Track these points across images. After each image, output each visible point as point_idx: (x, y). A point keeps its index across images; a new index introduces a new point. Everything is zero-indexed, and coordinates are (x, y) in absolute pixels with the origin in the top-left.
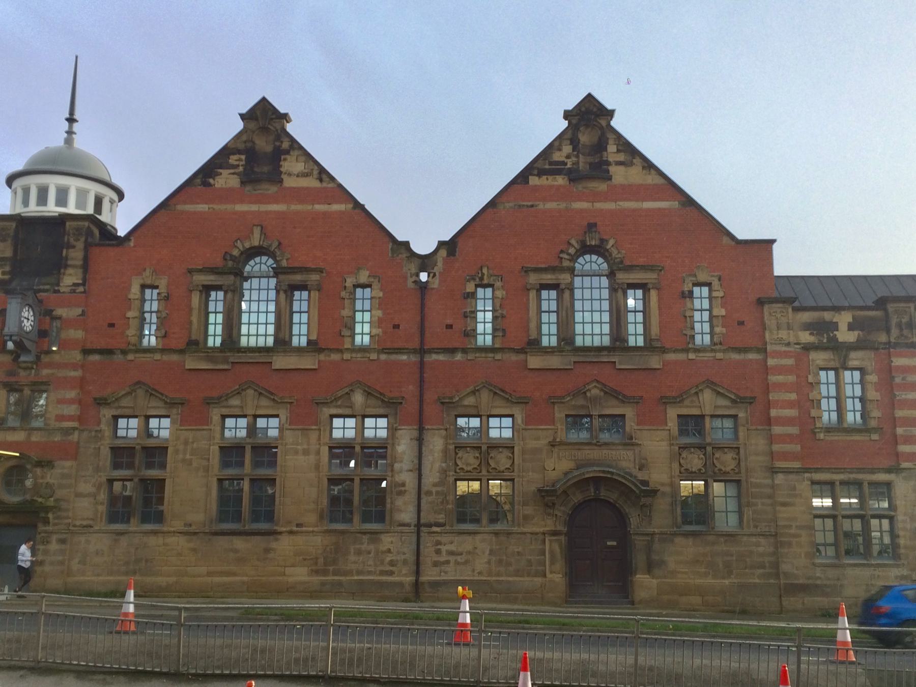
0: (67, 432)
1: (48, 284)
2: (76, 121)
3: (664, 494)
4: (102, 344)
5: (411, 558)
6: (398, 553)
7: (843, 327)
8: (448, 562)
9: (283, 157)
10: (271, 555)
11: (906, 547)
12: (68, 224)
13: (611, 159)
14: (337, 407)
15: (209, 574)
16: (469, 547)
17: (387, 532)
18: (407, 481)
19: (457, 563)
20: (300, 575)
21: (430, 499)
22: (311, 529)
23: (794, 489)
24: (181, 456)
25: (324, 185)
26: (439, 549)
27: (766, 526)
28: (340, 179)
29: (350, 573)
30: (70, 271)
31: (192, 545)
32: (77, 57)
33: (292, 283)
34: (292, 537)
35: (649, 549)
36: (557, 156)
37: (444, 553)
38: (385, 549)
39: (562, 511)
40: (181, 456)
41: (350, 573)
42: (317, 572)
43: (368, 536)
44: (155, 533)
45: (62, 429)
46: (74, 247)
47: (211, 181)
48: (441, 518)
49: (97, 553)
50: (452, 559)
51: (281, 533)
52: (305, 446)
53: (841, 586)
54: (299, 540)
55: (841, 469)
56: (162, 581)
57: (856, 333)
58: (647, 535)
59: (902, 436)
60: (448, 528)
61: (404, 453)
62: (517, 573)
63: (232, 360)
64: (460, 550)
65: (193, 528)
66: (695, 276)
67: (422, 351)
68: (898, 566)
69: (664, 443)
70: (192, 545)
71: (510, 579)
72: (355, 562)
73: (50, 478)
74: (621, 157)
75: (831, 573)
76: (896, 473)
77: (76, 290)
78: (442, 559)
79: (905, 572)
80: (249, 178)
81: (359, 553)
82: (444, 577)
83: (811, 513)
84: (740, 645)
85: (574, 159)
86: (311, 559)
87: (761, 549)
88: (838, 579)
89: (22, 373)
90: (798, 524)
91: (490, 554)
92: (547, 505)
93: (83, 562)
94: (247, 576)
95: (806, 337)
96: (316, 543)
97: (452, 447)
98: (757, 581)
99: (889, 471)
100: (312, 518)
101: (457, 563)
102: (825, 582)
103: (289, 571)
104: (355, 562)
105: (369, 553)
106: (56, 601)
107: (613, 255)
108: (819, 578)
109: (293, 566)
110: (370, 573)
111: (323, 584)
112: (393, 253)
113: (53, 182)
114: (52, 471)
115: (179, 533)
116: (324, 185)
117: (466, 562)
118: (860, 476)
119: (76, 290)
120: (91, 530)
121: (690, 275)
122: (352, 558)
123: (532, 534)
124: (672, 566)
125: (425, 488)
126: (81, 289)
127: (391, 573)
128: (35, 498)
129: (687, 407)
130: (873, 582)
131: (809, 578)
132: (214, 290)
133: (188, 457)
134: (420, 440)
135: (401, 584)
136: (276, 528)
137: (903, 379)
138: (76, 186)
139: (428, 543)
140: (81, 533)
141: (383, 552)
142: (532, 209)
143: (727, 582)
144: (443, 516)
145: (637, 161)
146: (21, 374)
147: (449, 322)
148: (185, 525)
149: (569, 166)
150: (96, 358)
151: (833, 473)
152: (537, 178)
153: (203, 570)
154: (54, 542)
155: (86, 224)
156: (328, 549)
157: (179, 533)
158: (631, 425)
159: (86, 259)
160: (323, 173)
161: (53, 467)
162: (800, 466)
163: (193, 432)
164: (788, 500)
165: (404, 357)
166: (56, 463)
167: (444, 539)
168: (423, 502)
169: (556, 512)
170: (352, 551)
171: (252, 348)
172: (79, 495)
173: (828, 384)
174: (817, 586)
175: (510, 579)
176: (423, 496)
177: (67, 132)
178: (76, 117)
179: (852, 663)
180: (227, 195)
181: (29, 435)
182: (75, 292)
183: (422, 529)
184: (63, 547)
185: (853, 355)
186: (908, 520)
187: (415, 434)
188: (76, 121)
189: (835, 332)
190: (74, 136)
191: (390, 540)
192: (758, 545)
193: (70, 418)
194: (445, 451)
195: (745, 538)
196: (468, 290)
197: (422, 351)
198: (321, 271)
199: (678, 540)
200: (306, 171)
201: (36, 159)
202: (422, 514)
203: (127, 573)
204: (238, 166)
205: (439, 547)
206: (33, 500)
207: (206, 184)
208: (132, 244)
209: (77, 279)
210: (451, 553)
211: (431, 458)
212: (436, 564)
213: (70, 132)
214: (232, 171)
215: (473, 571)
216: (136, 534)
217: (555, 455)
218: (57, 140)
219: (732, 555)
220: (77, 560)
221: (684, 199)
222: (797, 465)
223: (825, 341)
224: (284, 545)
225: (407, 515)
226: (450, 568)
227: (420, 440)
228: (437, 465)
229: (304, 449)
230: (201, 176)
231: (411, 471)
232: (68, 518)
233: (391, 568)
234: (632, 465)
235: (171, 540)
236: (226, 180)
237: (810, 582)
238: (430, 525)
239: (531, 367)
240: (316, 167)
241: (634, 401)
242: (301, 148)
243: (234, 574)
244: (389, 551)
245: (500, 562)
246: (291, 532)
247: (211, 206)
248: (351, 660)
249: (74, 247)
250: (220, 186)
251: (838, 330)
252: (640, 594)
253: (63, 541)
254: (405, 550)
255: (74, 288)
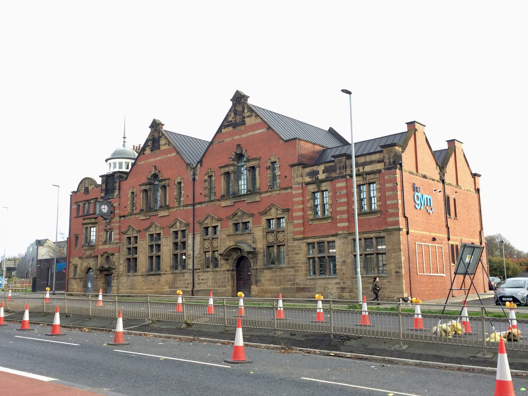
3: (261, 252)
7: (321, 172)
8: (201, 283)
10: (160, 282)
11: (339, 270)
13: (245, 116)
14: (174, 228)
15: (147, 289)
16: (206, 277)
19: (204, 283)
21: (197, 259)
23: (300, 247)
27: (292, 263)
35: (256, 276)
36: (230, 119)
37: (200, 280)
39: (231, 261)
43: (181, 274)
48: (199, 267)
50: (202, 281)
51: (161, 274)
53: (316, 288)
55: (315, 236)
57: (325, 174)
58: (255, 269)
59: (339, 219)
60: (201, 270)
61: (190, 243)
62: (219, 287)
64: (204, 278)
66: (271, 159)
68: (335, 278)
69: (261, 232)
74: (249, 114)
75: (312, 282)
76: (336, 236)
79: (338, 281)
81: (180, 280)
82: (200, 288)
83: (306, 257)
85: (234, 119)
87: (291, 273)
88: (314, 285)
90: (302, 262)
91: (212, 279)
92: (226, 260)
95: (308, 179)
96: (170, 277)
97: (202, 240)
98: (289, 287)
99: (333, 236)
100: (168, 269)
101: (204, 283)
102: (310, 286)
105: (182, 280)
108: (308, 285)
112: (187, 168)
118: (323, 239)
120: (123, 275)
121: (269, 159)
122: (178, 282)
123: (223, 271)
124: (263, 281)
125: (195, 256)
126: (118, 196)
129: (269, 216)
130: (326, 286)
131: (304, 285)
133: (142, 250)
134: (194, 238)
137: (340, 193)
139: (196, 275)
143: (279, 287)
144: (200, 266)
145: (254, 114)
147: (201, 192)
151: (314, 239)
153: (145, 288)
155: (119, 174)
158: (250, 225)
162: (302, 237)
164: (298, 252)
166: (115, 254)
167: (200, 274)
168: (195, 261)
169: (229, 262)
174: (307, 288)
176: (195, 259)
180: (149, 157)
183: (194, 271)
185: (323, 184)
186: (340, 258)
189: (318, 175)
190: (125, 143)
192: (290, 272)
194: (200, 241)
195: (286, 269)
196: (206, 179)
197: (194, 205)
198: (168, 179)
199: (265, 271)
201: (114, 154)
202: (195, 265)
207: (144, 154)
210: (202, 279)
211: (197, 244)
212: (199, 284)
215: (208, 286)
219: (282, 277)
221: (268, 127)
222: (302, 236)
223: (314, 180)
224: (163, 278)
225: (191, 267)
226: (201, 285)
227: (194, 238)
236: (148, 151)
237: (305, 286)
238: (196, 270)
241: (252, 215)
244: (187, 279)
245: (215, 282)
251: (319, 174)
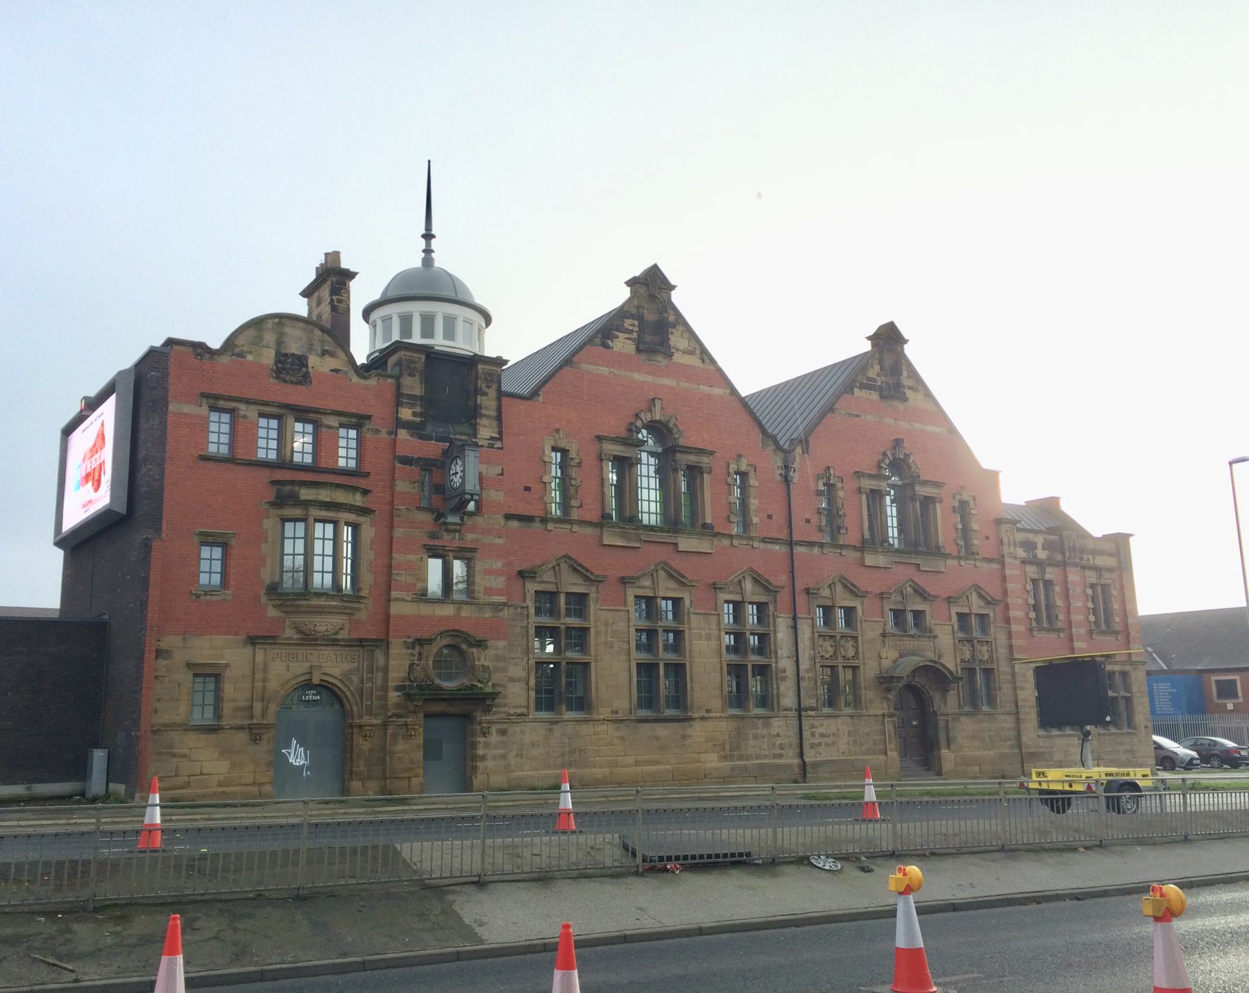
0: (497, 607)
1: (465, 434)
2: (433, 236)
4: (521, 510)
5: (794, 740)
6: (785, 736)
8: (820, 744)
9: (670, 330)
10: (687, 742)
12: (480, 366)
15: (637, 763)
17: (776, 717)
18: (787, 667)
19: (827, 744)
20: (711, 761)
22: (718, 715)
24: (603, 638)
25: (706, 366)
26: (814, 732)
28: (721, 363)
29: (748, 758)
30: (484, 421)
31: (619, 734)
32: (429, 162)
33: (689, 463)
34: (704, 723)
37: (817, 736)
38: (775, 733)
40: (603, 638)
41: (748, 758)
42: (725, 757)
44: (586, 721)
45: (493, 604)
46: (486, 394)
47: (610, 342)
49: (533, 745)
50: (822, 740)
51: (694, 719)
52: (707, 631)
54: (709, 725)
56: (599, 772)
63: (643, 538)
65: (620, 716)
67: (791, 544)
70: (619, 734)
71: (864, 757)
72: (753, 747)
73: (485, 661)
77: (493, 444)
78: (816, 741)
80: (642, 348)
81: (756, 737)
84: (150, 832)
86: (720, 745)
89: (446, 536)
91: (848, 735)
93: (520, 755)
94: (669, 764)
96: (722, 728)
98: (1008, 751)
100: (716, 704)
103: (703, 757)
104: (753, 747)
106: (668, 794)
107: (913, 469)
109: (706, 752)
110: (765, 757)
111: (733, 769)
113: (416, 309)
114: (486, 652)
115: (608, 720)
116: (706, 366)
117: (834, 743)
119: (493, 444)
122: (752, 743)
126: (498, 444)
127: (781, 756)
128: (475, 683)
132: (314, 429)
135: (790, 766)
136: (690, 714)
138: (419, 312)
140: (518, 723)
141: (774, 736)
142: (858, 419)
143: (991, 753)
146: (445, 538)
148: (613, 712)
149: (879, 383)
150: (514, 524)
152: (858, 390)
153: (631, 759)
154: (494, 733)
156: (732, 735)
157: (608, 720)
159: (499, 410)
160: (704, 354)
161: (487, 647)
163: (613, 612)
165: (777, 547)
167: (817, 723)
170: (751, 736)
171: (652, 526)
172: (512, 680)
173: (324, 539)
175: (864, 757)
177: (424, 251)
178: (433, 232)
179: (573, 832)
181: (459, 609)
182: (493, 447)
184: (504, 739)
187: (790, 622)
188: (433, 236)
191: (778, 724)
193: (498, 592)
199: (963, 719)
200: (690, 348)
203: (562, 766)
204: (632, 331)
205: (814, 730)
206: (472, 685)
208: (540, 399)
209: (493, 432)
210: (822, 735)
213: (428, 251)
214: (627, 336)
216: (568, 723)
217: (887, 645)
218: (416, 261)
220: (513, 754)
224: (697, 731)
225: (789, 700)
228: (807, 653)
229: (706, 634)
230: (600, 336)
231: (789, 657)
232: (505, 705)
233: (781, 751)
234: (933, 655)
235: (601, 728)
238: (806, 710)
239: (605, 543)
240: (698, 347)
242: (686, 324)
243: (659, 763)
244: (778, 735)
245: (855, 742)
246: (703, 718)
247: (611, 370)
248: (177, 866)
249: (486, 394)
250: (617, 350)
252: (947, 766)
253: (503, 732)
254: (790, 734)
255: (491, 442)
